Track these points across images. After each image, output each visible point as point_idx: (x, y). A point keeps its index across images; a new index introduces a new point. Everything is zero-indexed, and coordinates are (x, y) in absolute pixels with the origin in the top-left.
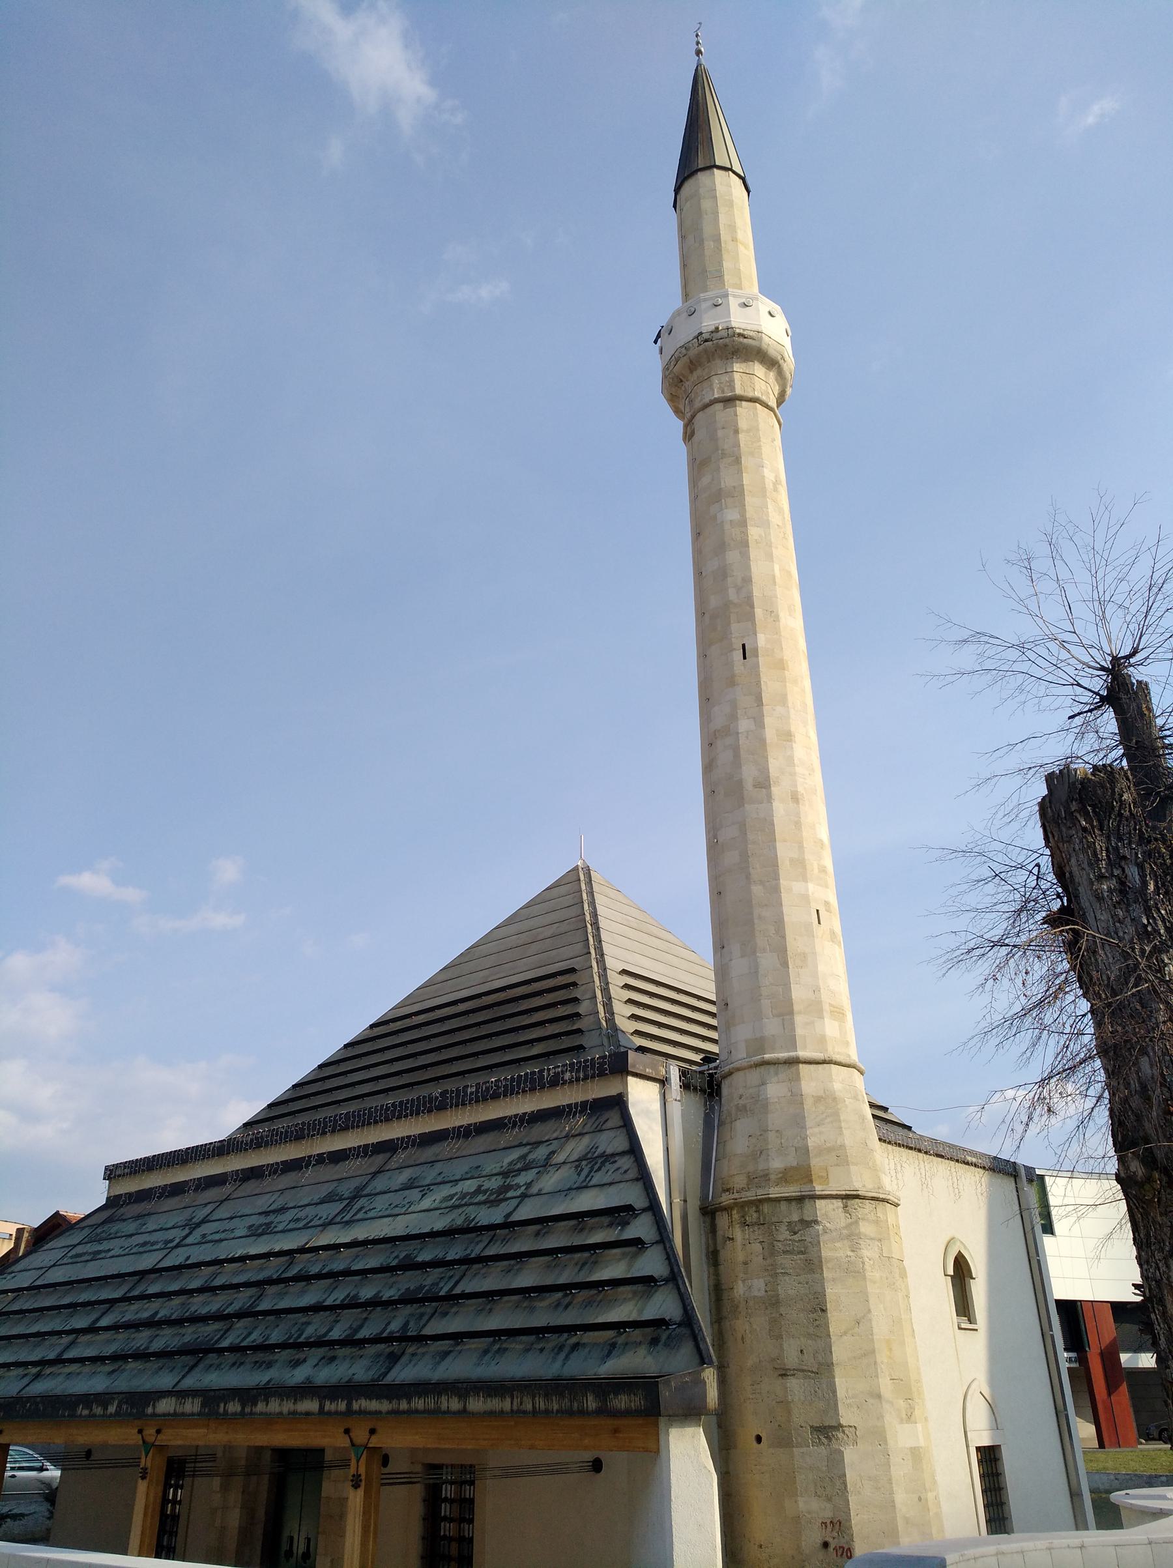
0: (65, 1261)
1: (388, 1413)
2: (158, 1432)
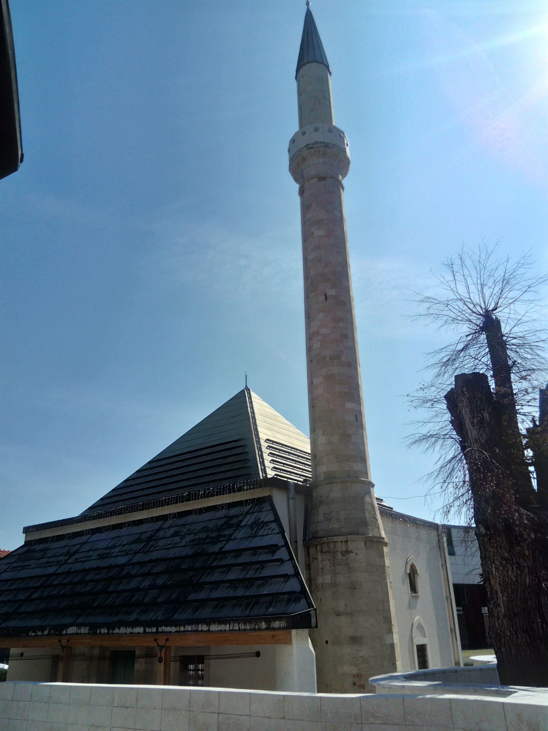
0: (9, 570)
1: (175, 632)
2: (68, 641)
